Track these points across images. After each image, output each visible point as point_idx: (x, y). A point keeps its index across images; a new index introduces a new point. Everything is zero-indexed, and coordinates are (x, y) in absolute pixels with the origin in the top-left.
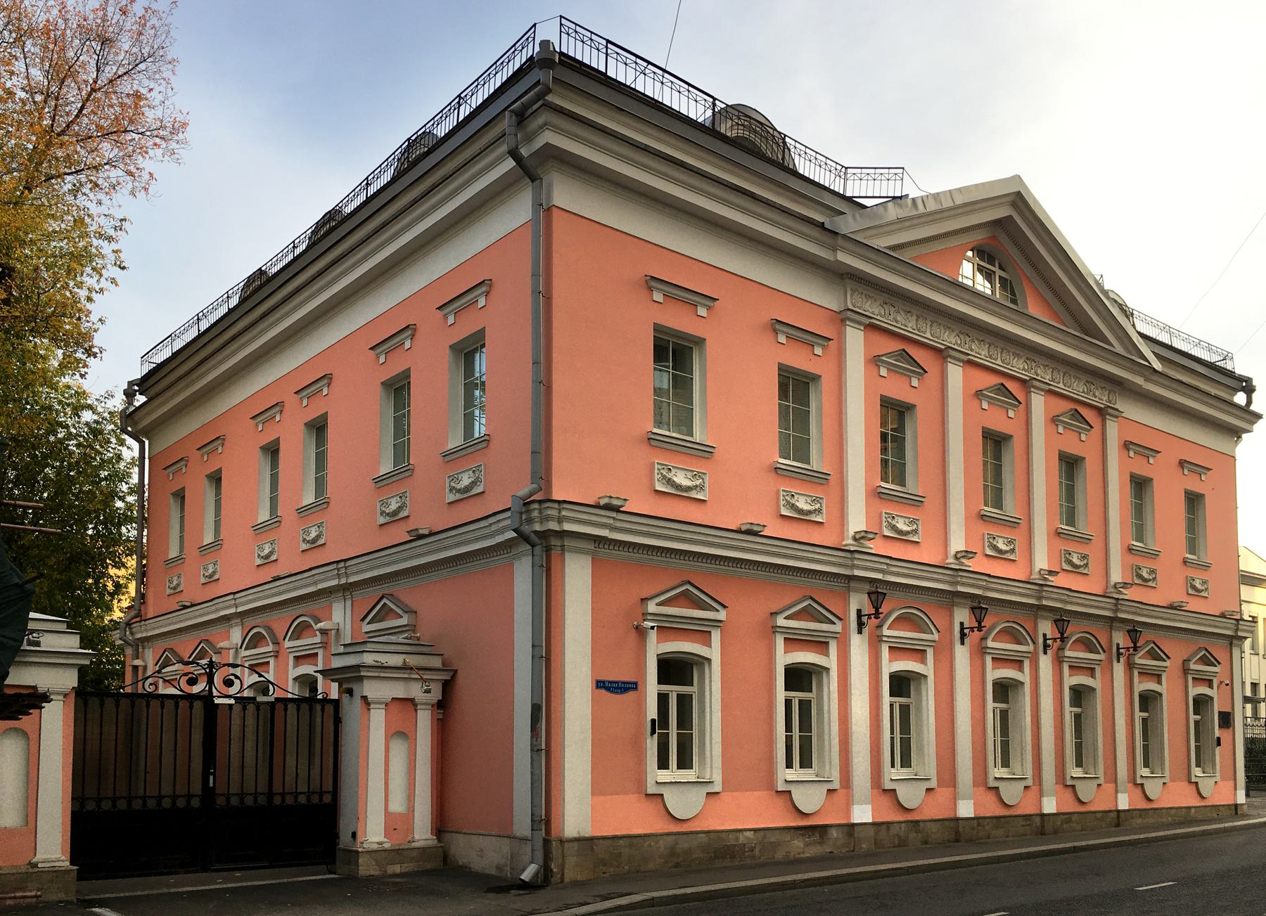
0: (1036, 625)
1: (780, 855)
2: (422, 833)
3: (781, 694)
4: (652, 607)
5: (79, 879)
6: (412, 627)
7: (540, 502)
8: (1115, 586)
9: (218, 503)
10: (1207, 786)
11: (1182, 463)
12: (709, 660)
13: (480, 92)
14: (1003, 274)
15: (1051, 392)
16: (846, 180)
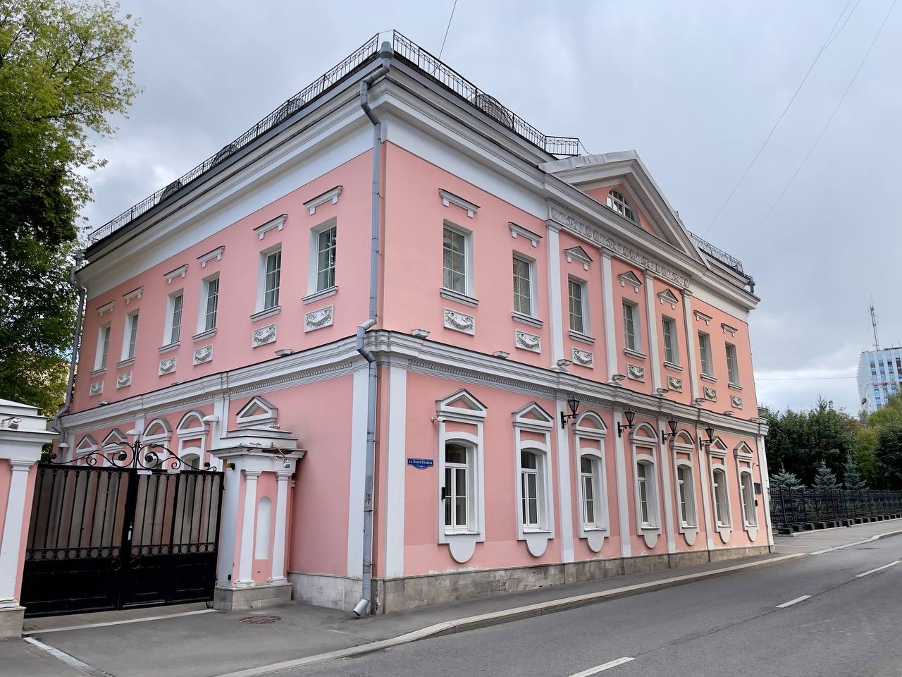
0: (657, 423)
1: (521, 587)
2: (277, 576)
3: (519, 470)
4: (443, 407)
5: (26, 617)
6: (275, 420)
7: (376, 331)
8: (696, 401)
9: (134, 332)
10: (725, 534)
11: (723, 325)
12: (476, 445)
13: (357, 60)
14: (628, 207)
15: (655, 278)
16: (545, 143)
